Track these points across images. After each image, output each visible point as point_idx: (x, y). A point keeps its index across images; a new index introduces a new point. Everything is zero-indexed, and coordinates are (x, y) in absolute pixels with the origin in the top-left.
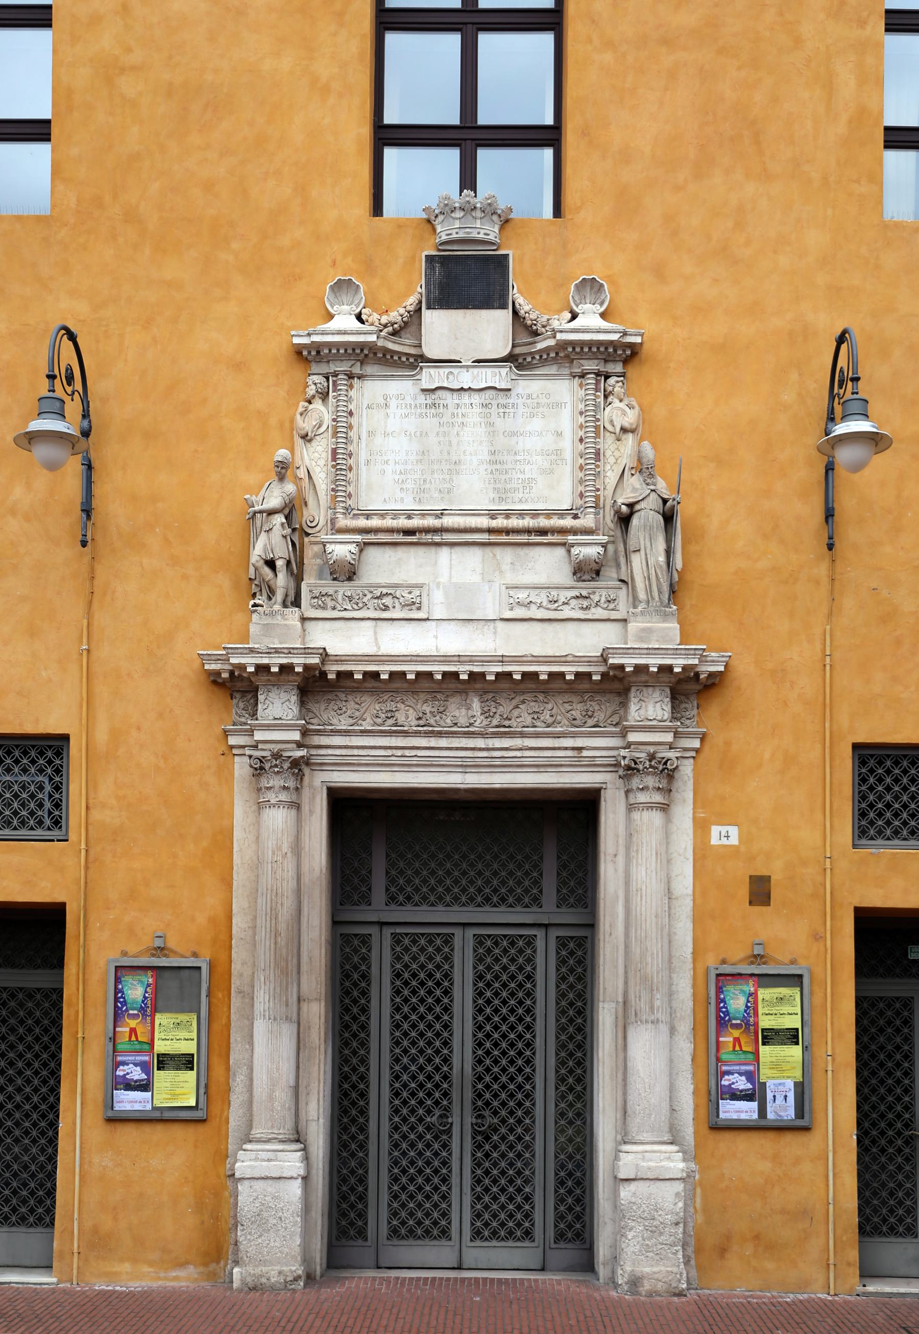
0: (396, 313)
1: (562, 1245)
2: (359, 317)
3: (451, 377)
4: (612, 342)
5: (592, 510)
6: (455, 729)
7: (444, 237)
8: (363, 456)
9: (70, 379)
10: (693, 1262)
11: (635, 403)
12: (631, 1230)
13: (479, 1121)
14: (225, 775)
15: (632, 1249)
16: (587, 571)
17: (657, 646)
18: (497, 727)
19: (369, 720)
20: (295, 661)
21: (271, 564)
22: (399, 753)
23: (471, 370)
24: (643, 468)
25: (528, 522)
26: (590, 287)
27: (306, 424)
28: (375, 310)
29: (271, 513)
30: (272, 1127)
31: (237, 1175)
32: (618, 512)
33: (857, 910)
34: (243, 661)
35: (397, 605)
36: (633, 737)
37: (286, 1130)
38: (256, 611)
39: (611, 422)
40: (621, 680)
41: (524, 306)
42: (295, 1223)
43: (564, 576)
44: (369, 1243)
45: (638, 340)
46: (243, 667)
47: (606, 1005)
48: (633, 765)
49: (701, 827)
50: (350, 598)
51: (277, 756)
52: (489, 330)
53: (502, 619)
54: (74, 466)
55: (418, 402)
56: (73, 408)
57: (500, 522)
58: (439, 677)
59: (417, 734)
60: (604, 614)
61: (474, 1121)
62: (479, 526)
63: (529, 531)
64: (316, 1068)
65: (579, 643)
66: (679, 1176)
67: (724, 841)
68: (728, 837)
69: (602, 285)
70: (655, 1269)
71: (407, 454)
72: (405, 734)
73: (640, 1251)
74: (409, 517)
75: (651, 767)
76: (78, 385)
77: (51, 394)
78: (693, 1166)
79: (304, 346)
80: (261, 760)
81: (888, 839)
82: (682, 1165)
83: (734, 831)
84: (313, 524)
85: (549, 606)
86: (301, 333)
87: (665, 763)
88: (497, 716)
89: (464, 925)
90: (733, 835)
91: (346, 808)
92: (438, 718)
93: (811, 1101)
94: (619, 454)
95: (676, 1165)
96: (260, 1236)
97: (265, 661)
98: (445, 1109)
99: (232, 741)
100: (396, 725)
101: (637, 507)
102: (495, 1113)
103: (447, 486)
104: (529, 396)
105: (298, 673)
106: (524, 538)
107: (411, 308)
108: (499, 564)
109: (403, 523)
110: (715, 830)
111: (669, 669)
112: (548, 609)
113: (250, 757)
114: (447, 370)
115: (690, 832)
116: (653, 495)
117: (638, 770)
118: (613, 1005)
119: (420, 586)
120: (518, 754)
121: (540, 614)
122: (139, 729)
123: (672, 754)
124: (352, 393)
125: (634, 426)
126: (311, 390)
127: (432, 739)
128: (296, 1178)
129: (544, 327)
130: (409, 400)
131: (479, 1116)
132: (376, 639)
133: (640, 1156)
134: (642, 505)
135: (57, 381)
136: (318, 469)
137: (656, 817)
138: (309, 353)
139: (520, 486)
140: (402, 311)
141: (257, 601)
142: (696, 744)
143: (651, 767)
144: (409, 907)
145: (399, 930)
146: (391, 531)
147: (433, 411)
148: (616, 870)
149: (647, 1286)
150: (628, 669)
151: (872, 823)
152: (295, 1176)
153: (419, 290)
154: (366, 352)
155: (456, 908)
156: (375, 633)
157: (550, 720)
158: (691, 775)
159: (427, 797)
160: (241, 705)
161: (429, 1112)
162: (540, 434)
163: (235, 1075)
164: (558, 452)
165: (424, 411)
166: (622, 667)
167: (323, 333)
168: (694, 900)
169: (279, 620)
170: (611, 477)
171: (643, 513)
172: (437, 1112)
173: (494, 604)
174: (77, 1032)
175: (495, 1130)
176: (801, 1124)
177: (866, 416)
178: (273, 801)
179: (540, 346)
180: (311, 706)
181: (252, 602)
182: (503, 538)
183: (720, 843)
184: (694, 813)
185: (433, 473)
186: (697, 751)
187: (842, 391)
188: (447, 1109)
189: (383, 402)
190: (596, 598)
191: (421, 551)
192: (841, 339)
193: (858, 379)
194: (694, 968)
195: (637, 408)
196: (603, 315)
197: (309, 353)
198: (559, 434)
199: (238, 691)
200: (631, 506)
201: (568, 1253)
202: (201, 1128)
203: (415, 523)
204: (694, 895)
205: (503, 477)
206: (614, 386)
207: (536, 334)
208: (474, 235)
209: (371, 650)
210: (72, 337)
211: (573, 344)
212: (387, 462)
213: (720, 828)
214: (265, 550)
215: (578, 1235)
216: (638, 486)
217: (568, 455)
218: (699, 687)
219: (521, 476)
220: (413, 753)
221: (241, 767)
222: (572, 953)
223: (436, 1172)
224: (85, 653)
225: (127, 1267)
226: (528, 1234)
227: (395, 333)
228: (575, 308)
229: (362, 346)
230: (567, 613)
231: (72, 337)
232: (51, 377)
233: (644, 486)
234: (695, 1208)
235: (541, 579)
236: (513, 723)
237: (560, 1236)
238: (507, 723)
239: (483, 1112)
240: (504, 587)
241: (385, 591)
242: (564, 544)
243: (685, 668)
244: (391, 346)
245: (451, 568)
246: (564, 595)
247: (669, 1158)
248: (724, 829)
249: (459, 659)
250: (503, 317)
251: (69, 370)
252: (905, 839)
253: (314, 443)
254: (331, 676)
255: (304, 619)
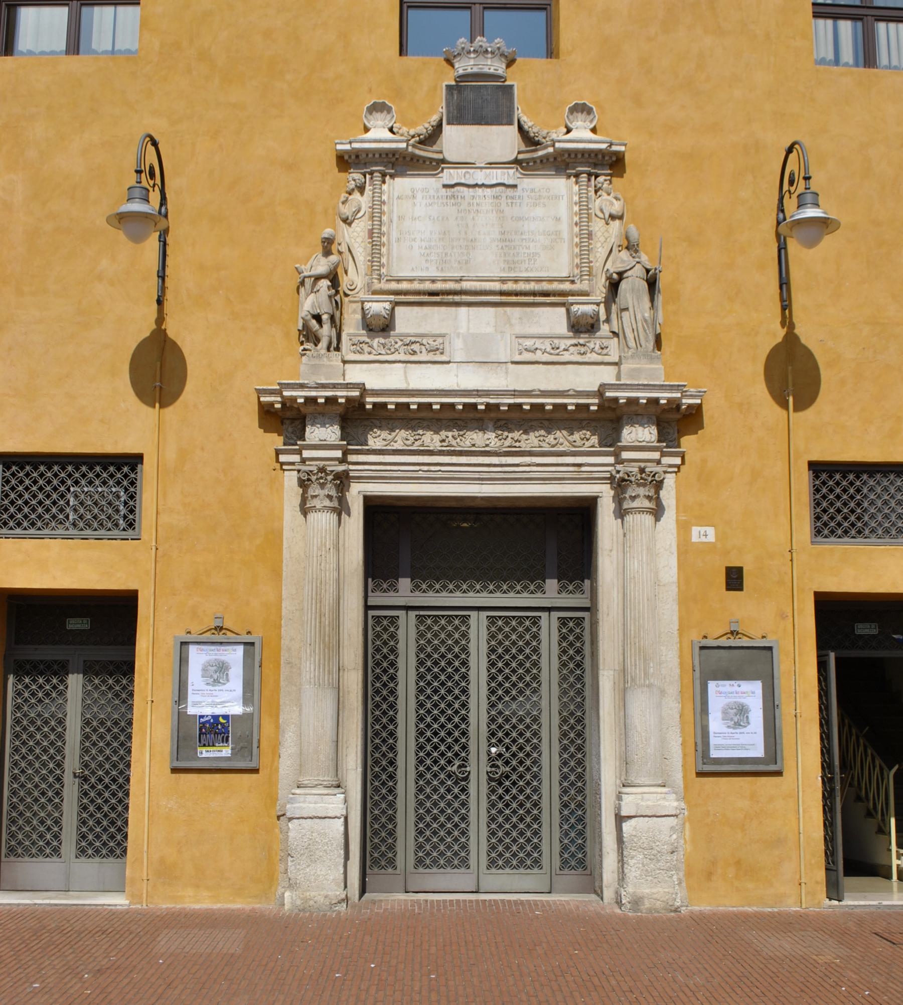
0: (422, 127)
1: (566, 871)
2: (391, 130)
3: (467, 176)
4: (601, 150)
5: (587, 277)
6: (473, 449)
7: (461, 72)
8: (394, 234)
9: (152, 175)
10: (684, 884)
11: (620, 196)
12: (632, 858)
13: (493, 769)
14: (277, 487)
15: (634, 874)
16: (584, 327)
17: (646, 383)
18: (509, 447)
19: (400, 442)
20: (339, 394)
21: (318, 318)
22: (425, 468)
23: (484, 170)
24: (631, 247)
25: (532, 286)
26: (581, 109)
27: (347, 210)
28: (404, 124)
29: (318, 278)
30: (318, 775)
31: (289, 815)
32: (609, 278)
33: (817, 595)
34: (294, 393)
35: (424, 350)
36: (625, 455)
37: (329, 779)
38: (305, 354)
39: (602, 211)
40: (614, 410)
41: (528, 123)
42: (339, 856)
43: (562, 327)
44: (398, 872)
45: (623, 148)
46: (294, 399)
47: (606, 673)
48: (626, 477)
49: (683, 528)
50: (384, 345)
51: (322, 470)
52: (502, 141)
53: (513, 363)
54: (152, 243)
55: (440, 195)
56: (155, 197)
57: (510, 286)
58: (461, 407)
59: (441, 453)
60: (599, 358)
61: (489, 769)
62: (493, 289)
63: (534, 294)
64: (355, 726)
65: (581, 378)
66: (674, 813)
67: (703, 539)
68: (706, 535)
69: (592, 109)
70: (654, 890)
71: (431, 233)
72: (431, 453)
73: (641, 875)
74: (433, 281)
75: (642, 478)
76: (158, 181)
77: (138, 185)
78: (683, 805)
79: (346, 152)
80: (309, 473)
81: (840, 537)
82: (675, 804)
83: (711, 531)
84: (352, 288)
85: (552, 351)
86: (344, 141)
87: (654, 476)
88: (509, 439)
89: (478, 605)
90: (710, 535)
91: (378, 512)
92: (458, 440)
93: (782, 750)
94: (607, 235)
95: (671, 803)
96: (308, 866)
97: (313, 394)
98: (463, 760)
99: (283, 458)
100: (423, 445)
101: (625, 275)
102: (507, 763)
103: (465, 258)
104: (533, 190)
105: (341, 403)
106: (530, 299)
107: (434, 124)
108: (509, 319)
109: (428, 286)
110: (695, 530)
111: (656, 401)
112: (551, 354)
113: (299, 471)
114: (464, 171)
115: (675, 531)
116: (638, 265)
117: (631, 482)
118: (612, 672)
119: (443, 336)
120: (527, 469)
121: (546, 358)
122: (202, 449)
123: (659, 469)
124: (385, 187)
125: (620, 214)
126: (352, 185)
127: (454, 457)
128: (339, 818)
129: (545, 138)
130: (432, 193)
131: (493, 766)
132: (406, 377)
133: (639, 796)
134: (629, 273)
135: (143, 175)
136: (356, 245)
137: (649, 519)
138: (350, 157)
139: (526, 259)
140: (427, 125)
141: (306, 347)
142: (678, 461)
143: (642, 478)
144: (431, 594)
145: (422, 613)
146: (418, 293)
147: (452, 201)
148: (612, 562)
149: (647, 904)
150: (621, 401)
151: (825, 524)
152: (339, 815)
153: (440, 110)
154: (397, 156)
155: (471, 594)
156: (405, 372)
157: (554, 442)
158: (674, 486)
159: (447, 504)
160: (290, 430)
161: (449, 762)
162: (542, 219)
163: (284, 732)
164: (558, 233)
165: (445, 201)
166: (616, 400)
167: (362, 141)
168: (679, 587)
169: (325, 361)
170: (600, 252)
171: (630, 279)
172: (457, 763)
173: (505, 350)
174: (147, 697)
175: (507, 777)
176: (768, 767)
177: (817, 205)
178: (318, 507)
179: (540, 153)
180: (349, 430)
181: (302, 348)
182: (514, 299)
183: (700, 540)
184: (677, 516)
185: (453, 248)
186: (678, 467)
187: (792, 189)
188: (465, 760)
189: (411, 194)
190: (591, 345)
191: (443, 309)
192: (790, 150)
193: (809, 178)
194: (681, 642)
195: (622, 201)
196: (594, 130)
197: (350, 157)
198: (558, 219)
199: (288, 419)
200: (621, 274)
201: (571, 877)
202: (254, 776)
203: (439, 286)
204: (679, 583)
205: (512, 252)
206: (603, 184)
207: (538, 143)
208: (486, 70)
209: (402, 385)
210: (155, 144)
211: (569, 152)
212: (414, 240)
213: (699, 528)
214: (313, 306)
215: (582, 863)
216: (625, 259)
217: (565, 235)
218: (678, 416)
219: (527, 251)
220: (438, 468)
221: (291, 479)
222: (571, 631)
223: (456, 811)
224: (158, 389)
225: (190, 892)
226: (537, 863)
227: (421, 142)
228: (569, 124)
229: (394, 152)
230: (567, 357)
231: (155, 144)
232: (139, 172)
233: (631, 258)
234: (685, 839)
235: (546, 331)
236: (522, 444)
237: (564, 864)
238: (517, 444)
239: (497, 762)
240: (514, 337)
241: (413, 339)
242: (563, 304)
243: (670, 400)
244: (417, 152)
245: (469, 322)
246: (564, 344)
247: (664, 798)
248: (703, 529)
249: (478, 393)
250: (512, 131)
251: (152, 169)
252: (853, 537)
253: (353, 225)
254: (369, 407)
255: (345, 362)
